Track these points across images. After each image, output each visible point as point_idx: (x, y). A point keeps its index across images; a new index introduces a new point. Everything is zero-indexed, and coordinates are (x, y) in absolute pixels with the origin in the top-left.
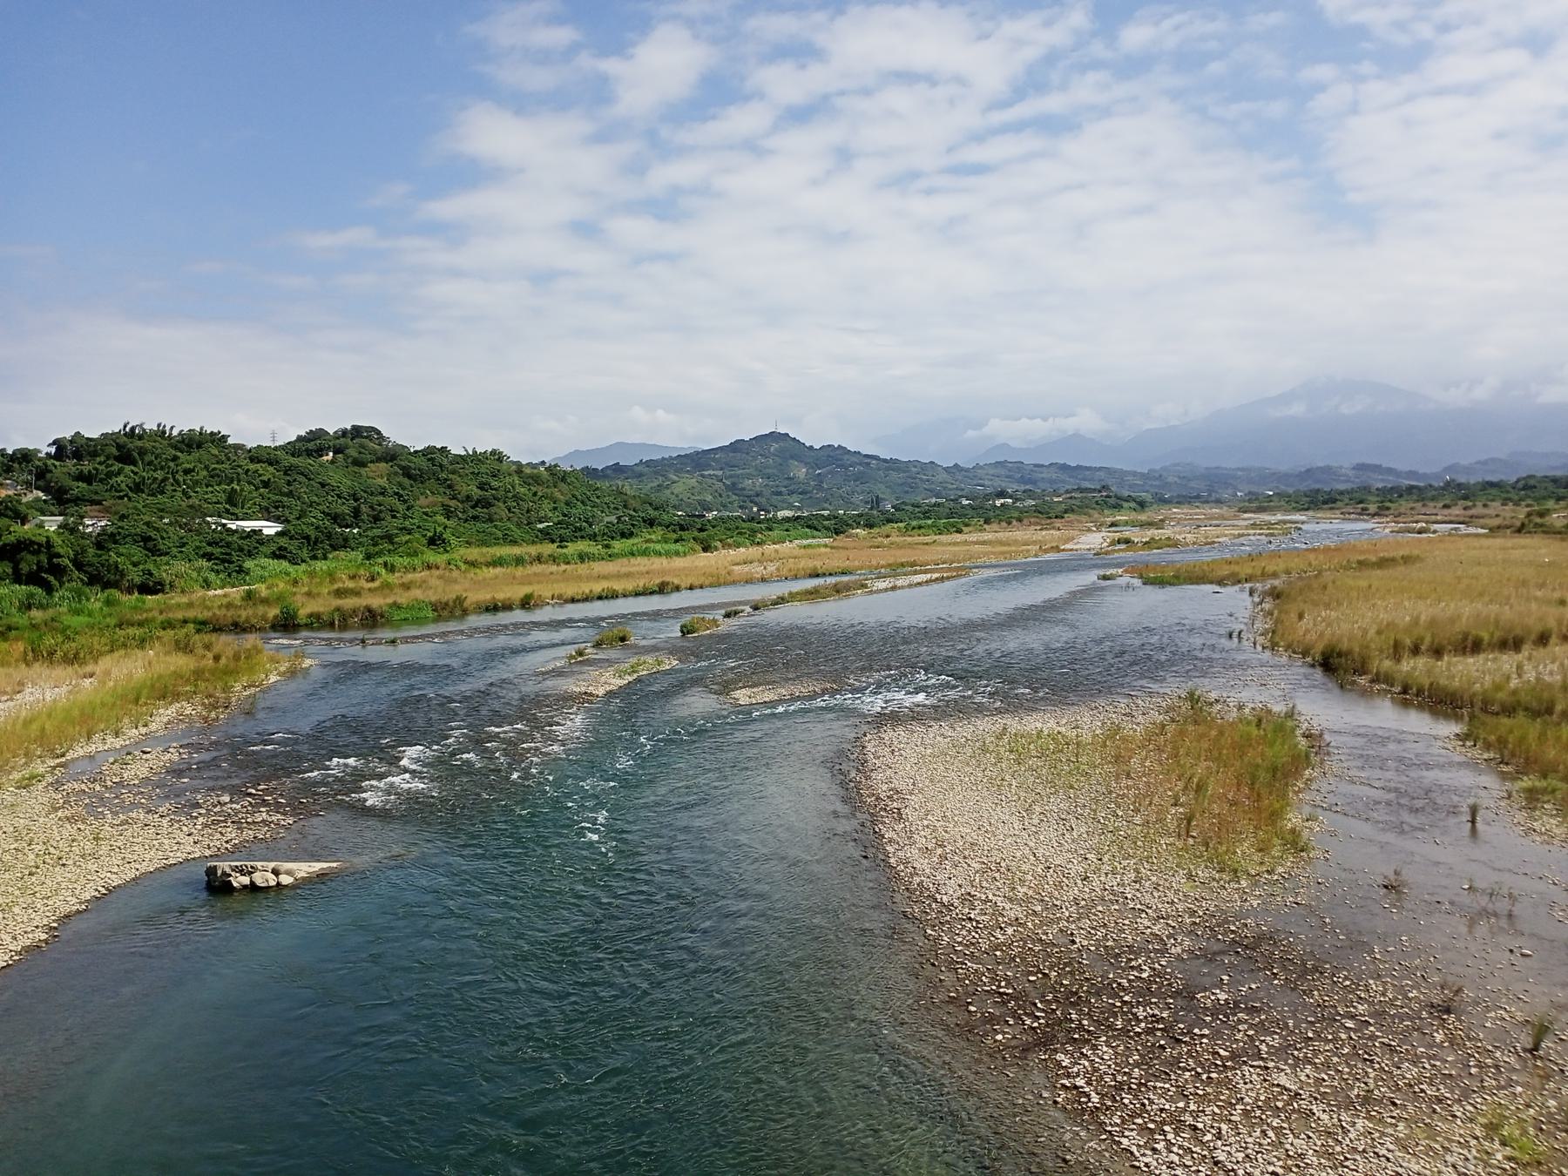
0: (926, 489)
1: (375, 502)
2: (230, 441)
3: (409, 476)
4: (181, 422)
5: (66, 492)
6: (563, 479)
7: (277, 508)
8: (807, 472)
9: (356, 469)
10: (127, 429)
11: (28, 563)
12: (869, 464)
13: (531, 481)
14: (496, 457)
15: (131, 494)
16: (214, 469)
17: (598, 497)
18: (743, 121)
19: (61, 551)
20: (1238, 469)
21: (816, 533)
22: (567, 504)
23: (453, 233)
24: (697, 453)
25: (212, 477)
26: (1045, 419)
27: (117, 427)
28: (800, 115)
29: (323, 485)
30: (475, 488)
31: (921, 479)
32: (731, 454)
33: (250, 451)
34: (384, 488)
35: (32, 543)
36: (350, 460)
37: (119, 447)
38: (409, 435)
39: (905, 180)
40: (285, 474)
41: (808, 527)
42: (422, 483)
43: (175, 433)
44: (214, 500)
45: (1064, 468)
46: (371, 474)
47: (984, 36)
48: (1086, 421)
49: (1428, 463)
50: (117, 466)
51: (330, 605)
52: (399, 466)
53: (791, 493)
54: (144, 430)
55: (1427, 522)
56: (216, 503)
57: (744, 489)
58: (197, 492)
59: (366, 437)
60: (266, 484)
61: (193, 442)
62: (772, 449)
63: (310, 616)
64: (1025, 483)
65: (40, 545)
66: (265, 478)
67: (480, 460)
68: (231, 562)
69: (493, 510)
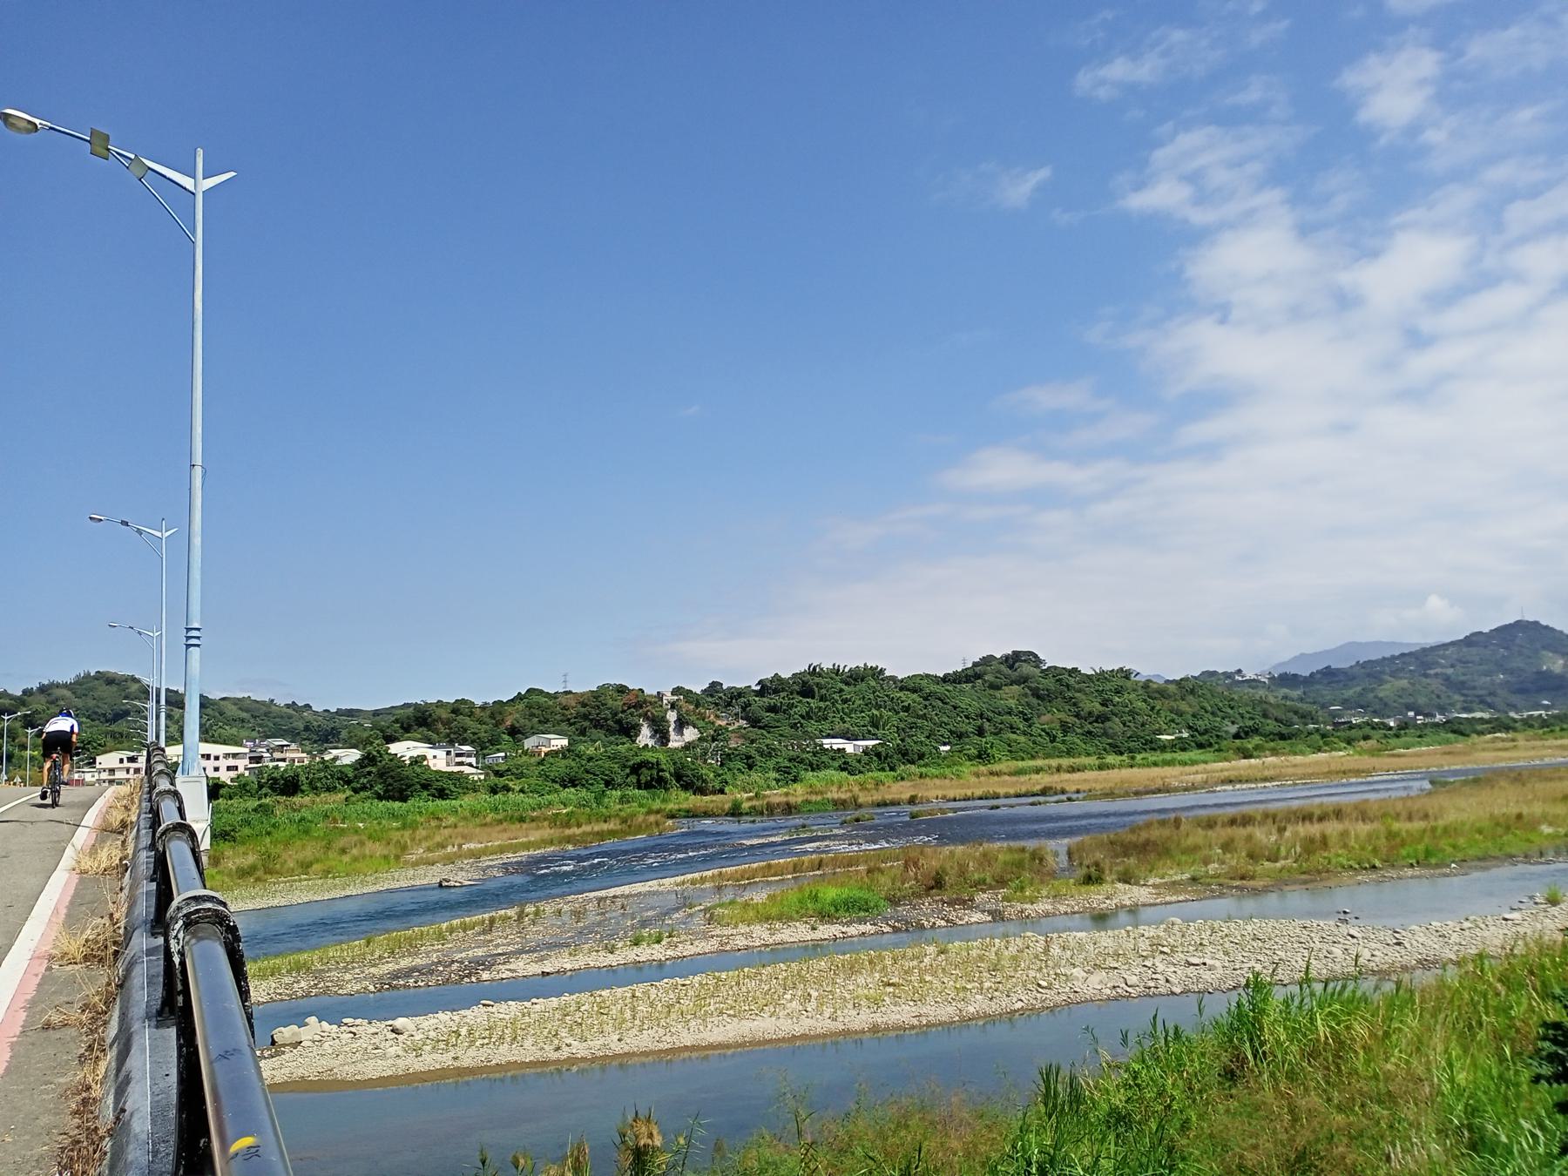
2: (887, 673)
3: (1039, 697)
4: (849, 663)
5: (759, 721)
6: (1192, 692)
7: (911, 728)
9: (992, 692)
11: (646, 775)
13: (1157, 695)
15: (802, 721)
17: (1232, 708)
18: (1504, 301)
19: (664, 767)
22: (1194, 716)
23: (1210, 451)
24: (1424, 650)
29: (955, 708)
30: (1098, 705)
32: (1465, 650)
33: (902, 681)
34: (1011, 708)
35: (649, 762)
36: (987, 685)
37: (805, 683)
40: (926, 699)
41: (1454, 732)
43: (846, 670)
46: (1005, 696)
51: (118, 726)
54: (822, 669)
57: (1474, 688)
59: (1025, 661)
60: (907, 709)
61: (856, 677)
63: (750, 808)
65: (653, 764)
66: (906, 704)
68: (789, 773)
69: (1108, 724)
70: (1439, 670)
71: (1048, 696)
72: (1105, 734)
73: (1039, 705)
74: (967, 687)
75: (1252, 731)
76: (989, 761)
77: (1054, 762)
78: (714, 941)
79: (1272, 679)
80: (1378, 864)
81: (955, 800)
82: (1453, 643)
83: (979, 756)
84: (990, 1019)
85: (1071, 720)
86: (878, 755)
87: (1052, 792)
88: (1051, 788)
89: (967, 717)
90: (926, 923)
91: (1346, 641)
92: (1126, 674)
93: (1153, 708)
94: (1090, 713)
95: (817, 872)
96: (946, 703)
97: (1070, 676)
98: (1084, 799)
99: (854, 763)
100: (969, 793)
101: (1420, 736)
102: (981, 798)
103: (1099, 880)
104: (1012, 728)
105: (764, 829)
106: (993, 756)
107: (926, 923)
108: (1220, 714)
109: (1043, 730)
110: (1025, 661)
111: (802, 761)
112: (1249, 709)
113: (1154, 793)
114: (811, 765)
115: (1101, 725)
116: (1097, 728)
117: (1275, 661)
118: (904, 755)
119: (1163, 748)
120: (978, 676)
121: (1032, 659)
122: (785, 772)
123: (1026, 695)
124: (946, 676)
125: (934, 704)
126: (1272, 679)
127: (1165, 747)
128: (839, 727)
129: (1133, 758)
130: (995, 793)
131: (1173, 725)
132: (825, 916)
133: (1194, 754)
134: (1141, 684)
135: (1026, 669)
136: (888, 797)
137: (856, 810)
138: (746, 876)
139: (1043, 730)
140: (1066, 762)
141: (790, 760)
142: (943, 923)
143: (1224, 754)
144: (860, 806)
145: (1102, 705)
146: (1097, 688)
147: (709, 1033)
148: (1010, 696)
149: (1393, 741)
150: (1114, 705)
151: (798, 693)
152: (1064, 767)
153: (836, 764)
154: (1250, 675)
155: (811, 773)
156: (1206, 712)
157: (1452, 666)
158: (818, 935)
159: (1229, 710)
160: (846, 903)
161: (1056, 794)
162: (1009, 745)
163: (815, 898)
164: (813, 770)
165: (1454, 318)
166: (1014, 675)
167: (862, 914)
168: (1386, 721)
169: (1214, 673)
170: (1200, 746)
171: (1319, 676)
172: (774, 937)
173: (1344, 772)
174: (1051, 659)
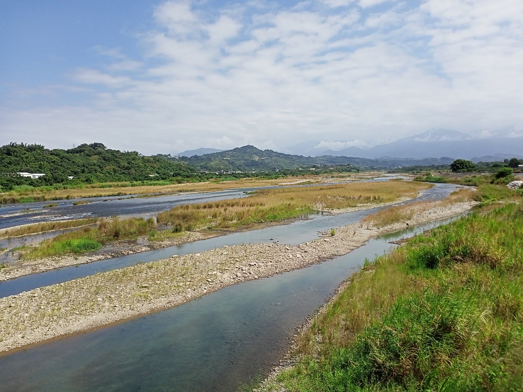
0: (297, 165)
1: (90, 168)
2: (45, 148)
3: (105, 160)
4: (28, 143)
6: (158, 161)
7: (56, 169)
8: (259, 159)
9: (87, 157)
10: (12, 144)
12: (280, 156)
13: (147, 161)
14: (136, 154)
16: (37, 157)
17: (170, 167)
18: (249, 46)
20: (405, 159)
21: (236, 179)
23: (159, 80)
25: (36, 160)
26: (342, 142)
27: (8, 143)
28: (269, 44)
29: (73, 162)
31: (296, 161)
33: (51, 151)
34: (95, 163)
36: (86, 154)
37: (8, 150)
38: (110, 145)
39: (299, 66)
40: (61, 159)
41: (235, 177)
42: (109, 162)
43: (27, 145)
44: (35, 167)
45: (346, 157)
46: (92, 159)
47: (323, 22)
48: (357, 143)
49: (395, 162)
50: (5, 156)
52: (102, 156)
53: (252, 165)
54: (17, 145)
55: (204, 192)
56: (35, 168)
57: (236, 164)
58: (30, 164)
59: (99, 147)
60: (54, 162)
61: (32, 149)
62: (248, 151)
64: (332, 163)
66: (53, 160)
67: (129, 155)
69: (130, 170)
70: (227, 158)
71: (109, 160)
72: (129, 174)
73: (105, 163)
74: (78, 155)
75: (178, 174)
76: (90, 182)
77: (116, 183)
78: (29, 268)
79: (179, 158)
80: (263, 221)
81: (85, 197)
82: (231, 151)
83: (87, 181)
84: (195, 299)
85: (117, 168)
86: (45, 180)
87: (121, 194)
88: (121, 193)
89: (78, 166)
90: (125, 253)
91: (201, 147)
92: (136, 154)
93: (145, 166)
94: (124, 166)
95: (53, 230)
96: (70, 161)
97: (117, 153)
98: (137, 197)
99: (36, 183)
100: (91, 195)
101: (226, 178)
102: (95, 197)
103: (180, 231)
104: (95, 171)
105: (10, 210)
106: (92, 180)
107: (125, 253)
108: (166, 168)
109: (107, 172)
110: (99, 147)
111: (13, 181)
112: (176, 167)
113: (161, 195)
114: (17, 183)
115: (128, 171)
116: (126, 171)
117: (183, 151)
118: (55, 180)
119: (151, 179)
120: (81, 151)
121: (101, 146)
122: (6, 186)
123: (100, 159)
124: (68, 150)
125: (65, 161)
126: (179, 158)
127: (152, 179)
128: (24, 168)
129: (143, 182)
130: (100, 195)
131: (152, 172)
132: (77, 252)
133: (161, 182)
134: (142, 157)
135: (100, 150)
136: (58, 196)
137: (44, 201)
138: (20, 233)
139: (107, 172)
140: (120, 183)
141: (7, 181)
142: (132, 252)
143: (172, 182)
144: (46, 200)
145: (128, 164)
146: (126, 158)
147: (72, 326)
148: (94, 159)
149: (219, 179)
150: (132, 164)
151: (6, 154)
152: (119, 185)
153: (28, 183)
154: (172, 156)
155: (17, 186)
156: (162, 168)
157: (230, 157)
158: (79, 262)
159: (169, 167)
160: (84, 246)
161: (123, 195)
162: (97, 177)
163: (70, 245)
164: (18, 185)
165: (234, 49)
166: (96, 151)
167: (93, 250)
168: (216, 173)
169: (161, 155)
170: (163, 179)
171: (193, 158)
172: (58, 264)
173: (218, 189)
174: (109, 146)
